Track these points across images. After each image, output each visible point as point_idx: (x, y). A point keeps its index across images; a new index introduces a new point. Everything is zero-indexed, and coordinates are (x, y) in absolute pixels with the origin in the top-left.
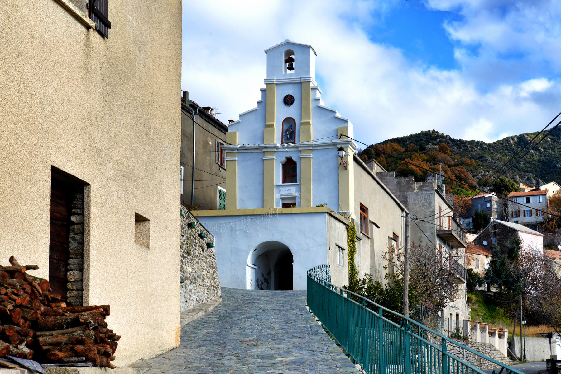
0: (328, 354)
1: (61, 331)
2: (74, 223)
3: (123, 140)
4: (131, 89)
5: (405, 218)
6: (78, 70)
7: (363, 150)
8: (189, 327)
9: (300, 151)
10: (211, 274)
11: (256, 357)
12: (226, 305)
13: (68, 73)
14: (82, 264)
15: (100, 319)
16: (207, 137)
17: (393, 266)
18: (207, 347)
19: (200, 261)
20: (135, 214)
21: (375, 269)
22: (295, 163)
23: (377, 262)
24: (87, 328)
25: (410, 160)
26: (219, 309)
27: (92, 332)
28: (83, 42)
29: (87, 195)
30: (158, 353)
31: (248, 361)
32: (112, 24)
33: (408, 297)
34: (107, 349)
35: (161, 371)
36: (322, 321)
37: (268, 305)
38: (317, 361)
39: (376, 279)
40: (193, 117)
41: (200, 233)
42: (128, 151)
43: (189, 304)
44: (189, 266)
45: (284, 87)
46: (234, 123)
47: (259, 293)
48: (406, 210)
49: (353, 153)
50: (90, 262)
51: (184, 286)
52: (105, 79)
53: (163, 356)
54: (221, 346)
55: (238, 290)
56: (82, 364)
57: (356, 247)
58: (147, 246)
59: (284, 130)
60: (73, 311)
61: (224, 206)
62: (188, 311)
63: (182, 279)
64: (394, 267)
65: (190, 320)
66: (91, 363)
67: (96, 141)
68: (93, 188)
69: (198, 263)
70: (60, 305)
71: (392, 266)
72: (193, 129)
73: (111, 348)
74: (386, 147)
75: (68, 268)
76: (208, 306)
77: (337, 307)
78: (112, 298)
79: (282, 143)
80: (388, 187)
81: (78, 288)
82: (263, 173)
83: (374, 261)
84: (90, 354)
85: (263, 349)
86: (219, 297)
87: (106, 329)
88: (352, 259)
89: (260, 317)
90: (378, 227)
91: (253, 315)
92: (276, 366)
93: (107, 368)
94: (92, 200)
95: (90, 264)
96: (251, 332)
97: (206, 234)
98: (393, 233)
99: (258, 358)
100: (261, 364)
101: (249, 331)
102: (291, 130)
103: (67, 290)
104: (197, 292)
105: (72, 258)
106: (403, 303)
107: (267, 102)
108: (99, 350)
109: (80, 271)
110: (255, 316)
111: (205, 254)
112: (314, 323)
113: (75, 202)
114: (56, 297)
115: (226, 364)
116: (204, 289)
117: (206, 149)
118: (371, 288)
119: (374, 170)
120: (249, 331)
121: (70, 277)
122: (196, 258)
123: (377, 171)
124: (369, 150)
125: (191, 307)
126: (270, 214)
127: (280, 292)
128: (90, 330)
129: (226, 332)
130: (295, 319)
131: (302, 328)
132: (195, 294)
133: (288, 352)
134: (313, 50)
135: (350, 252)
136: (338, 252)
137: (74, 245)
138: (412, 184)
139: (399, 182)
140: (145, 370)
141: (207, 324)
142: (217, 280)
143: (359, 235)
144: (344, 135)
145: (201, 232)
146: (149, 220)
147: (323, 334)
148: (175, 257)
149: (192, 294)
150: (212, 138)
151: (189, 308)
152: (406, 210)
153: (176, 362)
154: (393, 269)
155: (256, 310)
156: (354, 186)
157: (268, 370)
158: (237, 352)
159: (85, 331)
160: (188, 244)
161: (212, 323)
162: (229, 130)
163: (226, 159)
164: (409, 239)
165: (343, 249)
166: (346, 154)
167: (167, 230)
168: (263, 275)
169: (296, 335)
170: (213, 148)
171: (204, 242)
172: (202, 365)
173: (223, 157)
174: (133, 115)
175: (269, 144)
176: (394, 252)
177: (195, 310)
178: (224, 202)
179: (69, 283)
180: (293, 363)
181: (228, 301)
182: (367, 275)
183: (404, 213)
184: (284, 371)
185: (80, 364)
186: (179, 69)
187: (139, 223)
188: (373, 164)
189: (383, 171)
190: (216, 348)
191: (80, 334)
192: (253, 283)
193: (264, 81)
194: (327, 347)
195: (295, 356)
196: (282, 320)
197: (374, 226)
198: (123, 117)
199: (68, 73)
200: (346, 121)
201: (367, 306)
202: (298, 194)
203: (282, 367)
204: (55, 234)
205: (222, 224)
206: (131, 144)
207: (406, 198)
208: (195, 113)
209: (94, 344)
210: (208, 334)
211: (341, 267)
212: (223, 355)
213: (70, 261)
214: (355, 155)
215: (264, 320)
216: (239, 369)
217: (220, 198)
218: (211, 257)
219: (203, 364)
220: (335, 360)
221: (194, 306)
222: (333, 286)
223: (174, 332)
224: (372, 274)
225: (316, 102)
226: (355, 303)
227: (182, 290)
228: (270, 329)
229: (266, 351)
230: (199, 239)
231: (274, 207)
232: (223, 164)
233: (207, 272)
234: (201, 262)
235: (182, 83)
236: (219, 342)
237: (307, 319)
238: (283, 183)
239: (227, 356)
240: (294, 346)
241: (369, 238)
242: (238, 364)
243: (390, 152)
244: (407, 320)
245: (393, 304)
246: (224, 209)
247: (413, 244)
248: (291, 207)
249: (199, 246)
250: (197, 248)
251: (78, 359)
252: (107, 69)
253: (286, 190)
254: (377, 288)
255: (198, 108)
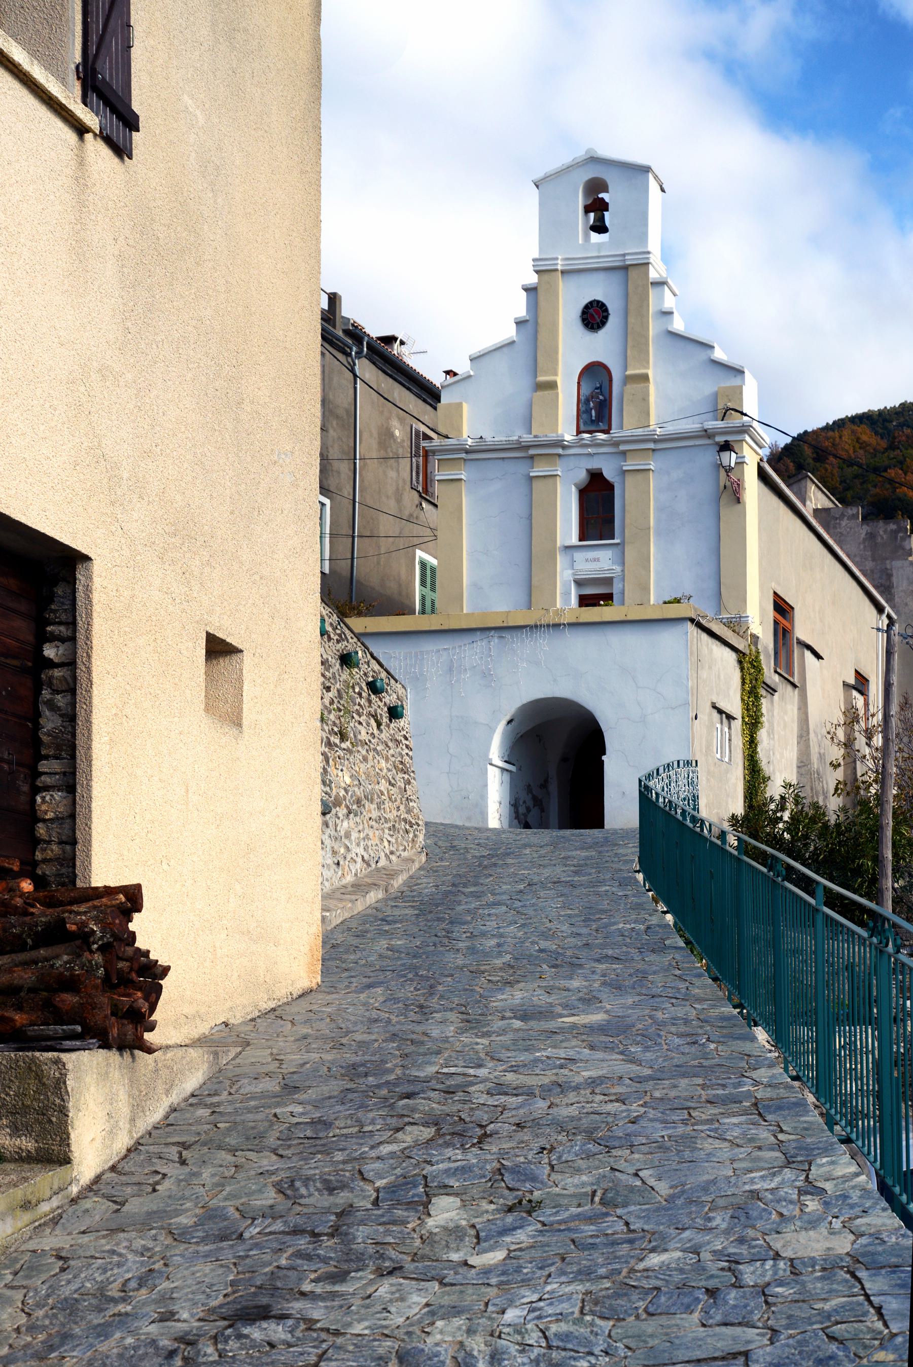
0: (688, 1003)
1: (19, 955)
2: (50, 664)
3: (174, 435)
4: (193, 297)
5: (885, 635)
6: (56, 248)
7: (782, 445)
8: (343, 933)
9: (624, 453)
10: (400, 788)
11: (508, 1014)
12: (436, 871)
13: (32, 257)
14: (74, 774)
15: (117, 921)
16: (389, 418)
17: (855, 762)
18: (388, 988)
19: (371, 754)
20: (204, 636)
21: (809, 770)
22: (610, 487)
23: (814, 750)
24: (85, 948)
25: (900, 472)
26: (419, 881)
27: (98, 958)
28: (68, 171)
29: (84, 586)
30: (265, 1006)
31: (488, 1024)
32: (141, 119)
33: (890, 845)
34: (136, 1000)
35: (272, 1054)
36: (675, 914)
37: (541, 870)
38: (661, 1024)
39: (812, 797)
40: (355, 364)
41: (370, 679)
42: (186, 465)
43: (343, 870)
44: (344, 769)
45: (584, 279)
46: (456, 378)
47: (518, 838)
48: (888, 609)
49: (757, 458)
50: (94, 768)
51: (330, 824)
52: (125, 269)
53: (277, 1013)
54: (423, 984)
55: (468, 828)
56: (74, 1043)
57: (764, 710)
58: (236, 720)
59: (582, 398)
60: (50, 903)
61: (433, 602)
62: (342, 891)
63: (324, 803)
64: (858, 763)
65: (347, 915)
66: (94, 1041)
67: (104, 442)
68: (98, 567)
69: (365, 759)
70: (19, 886)
71: (851, 760)
72: (353, 396)
73: (146, 999)
74: (841, 437)
75: (39, 783)
76: (391, 875)
77: (712, 877)
78: (149, 863)
79: (579, 432)
80: (844, 547)
81: (64, 838)
82: (531, 515)
83: (808, 746)
84: (94, 1016)
85: (527, 991)
86: (419, 850)
87: (132, 949)
88: (752, 743)
89: (520, 904)
90: (818, 656)
91: (504, 897)
92: (560, 1037)
93: (137, 1052)
94: (95, 601)
95: (93, 773)
96: (499, 945)
97: (387, 681)
98: (856, 671)
99: (515, 1017)
100: (521, 1034)
101: (493, 942)
102: (601, 397)
103: (35, 842)
104: (364, 839)
105: (46, 757)
106: (878, 860)
107: (539, 321)
108: (116, 1005)
109: (68, 792)
110: (508, 902)
111: (384, 736)
112: (654, 920)
113: (53, 607)
114: (6, 865)
115: (435, 1033)
116: (383, 829)
117: (386, 451)
118: (799, 821)
119: (808, 503)
120: (493, 942)
121: (44, 807)
122: (362, 746)
123: (816, 504)
124: (799, 445)
125: (349, 879)
126: (548, 626)
127: (573, 835)
128: (91, 952)
129: (435, 945)
130: (609, 908)
131: (626, 934)
132: (358, 845)
133: (589, 1001)
134: (656, 177)
135: (747, 724)
136: (719, 726)
137: (53, 721)
138: (903, 539)
139: (871, 533)
140: (233, 1051)
141: (388, 923)
142: (415, 805)
143: (770, 678)
144: (733, 409)
145: (373, 677)
146: (241, 651)
147: (676, 948)
148: (308, 749)
149: (351, 844)
150: (401, 421)
151: (344, 882)
152: (888, 609)
153: (310, 1031)
154: (855, 768)
155: (510, 884)
156: (760, 547)
157: (539, 1050)
158: (463, 1002)
159: (79, 956)
160: (340, 710)
161: (401, 922)
162: (445, 399)
163: (437, 478)
164: (895, 689)
165: (730, 717)
166: (739, 460)
167: (286, 676)
168: (529, 789)
169: (610, 952)
170: (403, 447)
171: (381, 704)
172: (373, 1037)
173: (429, 471)
174: (199, 367)
175: (546, 436)
176: (858, 722)
177: (359, 888)
178: (431, 593)
179: (40, 825)
180: (601, 1029)
181: (441, 859)
182: (790, 786)
183: (884, 617)
184: (579, 1053)
185: (68, 1044)
186: (314, 238)
187: (216, 658)
188: (806, 487)
189: (831, 505)
190: (408, 992)
191: (66, 963)
192: (506, 809)
193: (532, 263)
194: (688, 985)
195: (607, 1012)
196: (576, 912)
197: (808, 654)
198: (174, 374)
199: (32, 257)
200: (739, 372)
201: (787, 878)
202: (618, 568)
203: (574, 1042)
204: (4, 693)
205: (428, 653)
206: (194, 446)
207: (890, 576)
208: (359, 354)
209: (104, 991)
210: (389, 953)
211: (724, 766)
212: (427, 1011)
213: (43, 766)
214: (762, 464)
215: (531, 912)
216: (467, 1049)
217: (423, 583)
218: (398, 742)
219: (377, 1034)
220: (706, 1022)
221: (356, 875)
222: (703, 822)
223: (305, 949)
224: (804, 781)
225: (665, 318)
226: (757, 869)
227: (327, 834)
228: (545, 935)
229: (535, 999)
230: (369, 695)
231: (558, 606)
232: (430, 489)
233: (390, 784)
234: (374, 758)
235: (322, 277)
236: (417, 974)
237: (638, 907)
238: (580, 540)
239: (436, 1012)
240: (604, 984)
241: (794, 686)
242: (463, 1033)
243: (851, 452)
244: (885, 919)
245: (853, 862)
246: (433, 612)
247: (906, 699)
248: (600, 605)
249: (370, 714)
250: (363, 719)
251: (63, 1030)
252: (131, 242)
253: (587, 560)
254: (813, 820)
255: (366, 339)
